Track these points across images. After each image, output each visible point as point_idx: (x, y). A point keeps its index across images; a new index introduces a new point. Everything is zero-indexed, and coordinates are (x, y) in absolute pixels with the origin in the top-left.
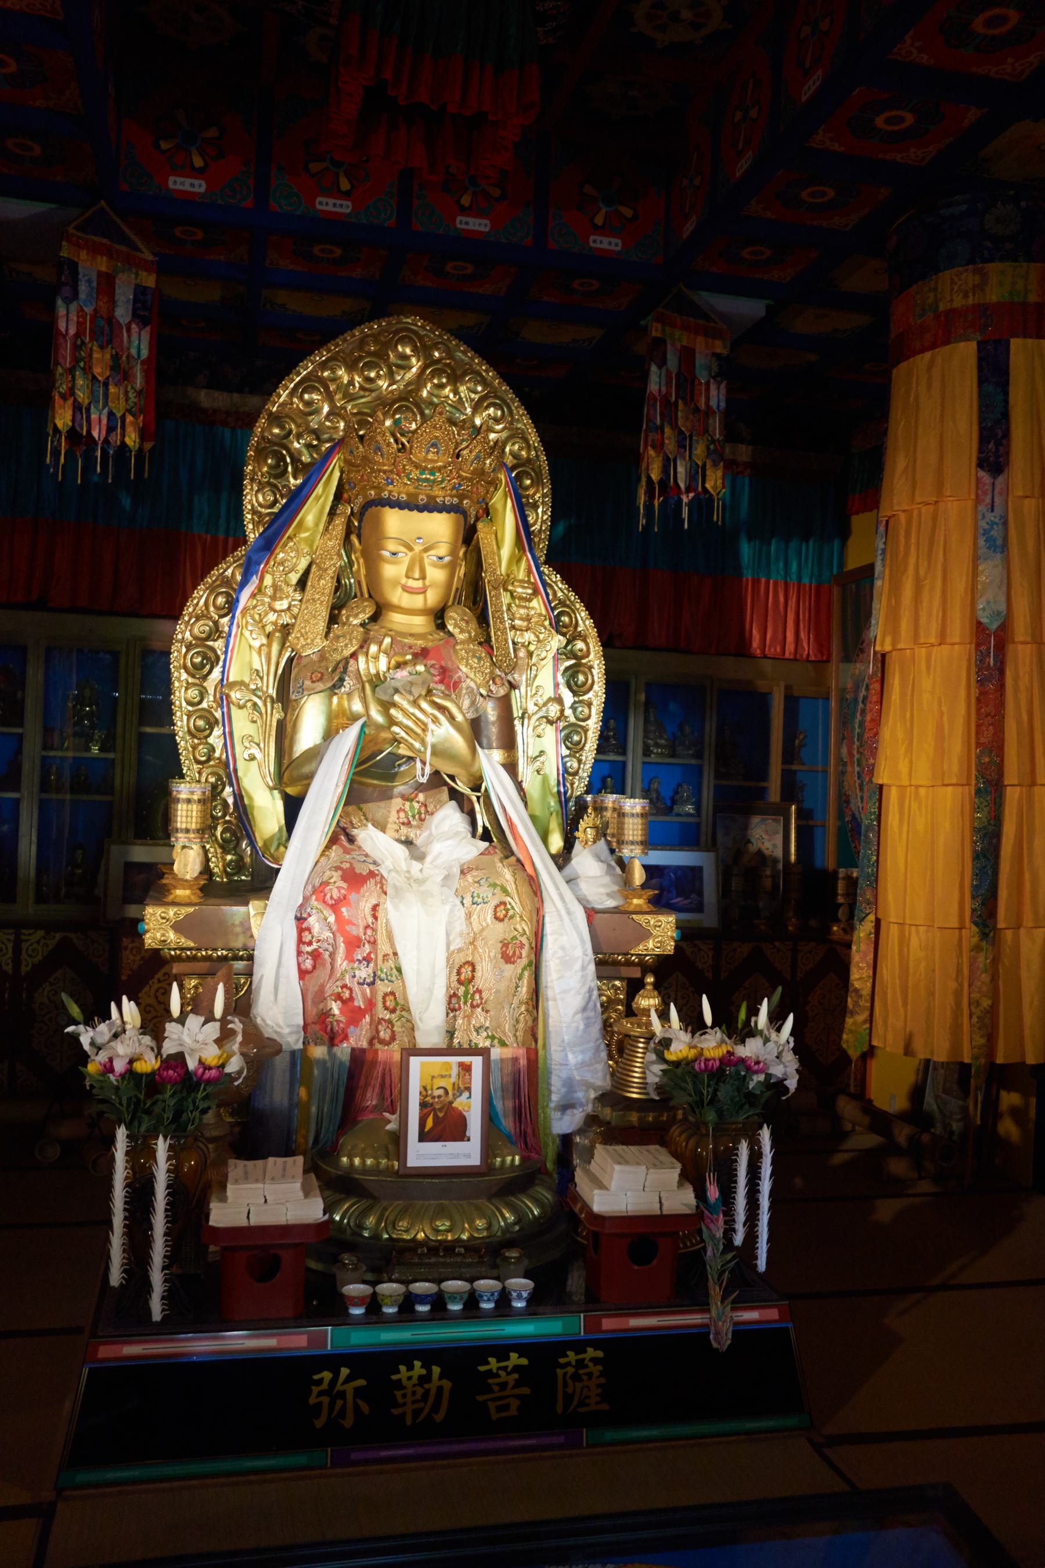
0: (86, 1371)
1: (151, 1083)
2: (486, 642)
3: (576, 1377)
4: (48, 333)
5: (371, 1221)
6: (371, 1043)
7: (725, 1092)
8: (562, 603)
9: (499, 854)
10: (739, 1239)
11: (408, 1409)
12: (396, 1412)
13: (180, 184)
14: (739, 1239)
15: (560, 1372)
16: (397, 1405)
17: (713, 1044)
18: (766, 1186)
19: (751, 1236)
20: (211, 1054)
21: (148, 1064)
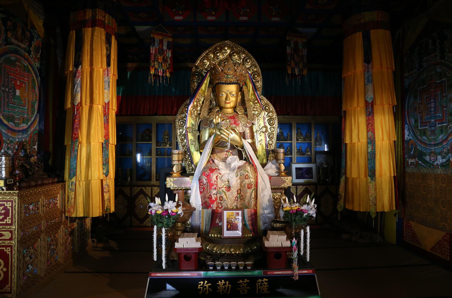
0: (149, 279)
1: (161, 216)
2: (247, 115)
3: (261, 285)
4: (149, 53)
5: (215, 249)
6: (216, 208)
7: (298, 218)
8: (266, 104)
9: (248, 164)
10: (302, 253)
11: (221, 291)
12: (218, 291)
13: (177, 18)
14: (302, 253)
15: (257, 284)
16: (218, 290)
17: (296, 206)
18: (308, 241)
19: (305, 253)
20: (174, 210)
21: (160, 212)
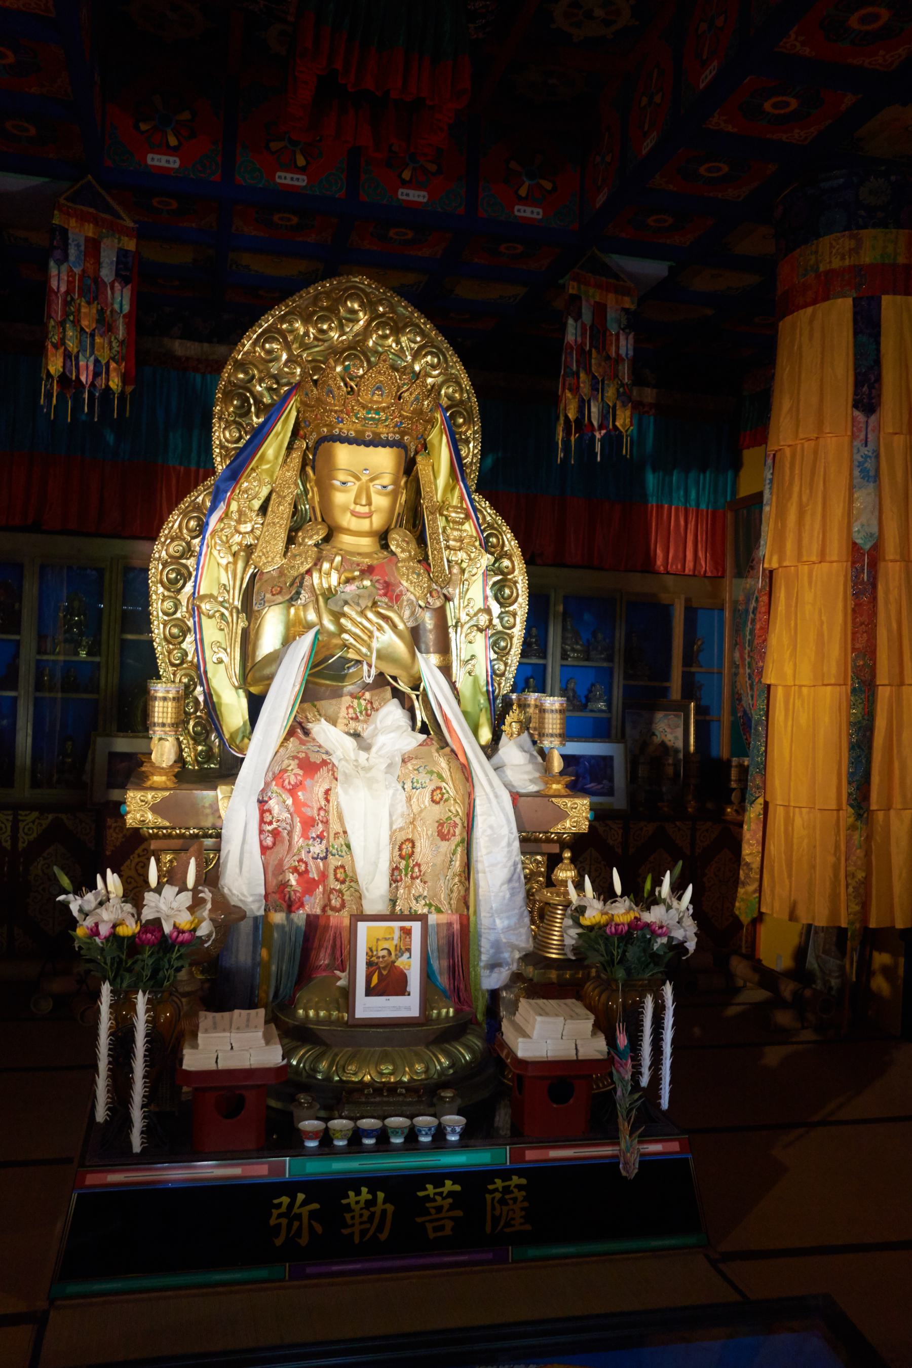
0: (75, 1196)
1: (132, 945)
2: (424, 561)
3: (503, 1202)
4: (42, 290)
5: (323, 1065)
6: (324, 910)
7: (633, 953)
8: (490, 526)
9: (436, 745)
10: (645, 1081)
11: (356, 1230)
12: (345, 1231)
13: (157, 160)
14: (645, 1081)
15: (488, 1197)
16: (347, 1226)
17: (623, 911)
18: (668, 1035)
19: (656, 1079)
20: (184, 920)
21: (130, 928)
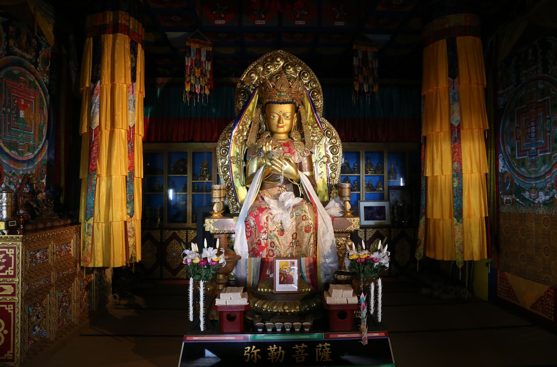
0: (183, 343)
1: (198, 266)
2: (304, 142)
3: (322, 351)
4: (183, 66)
5: (265, 306)
6: (267, 256)
7: (367, 268)
8: (328, 128)
9: (306, 202)
10: (372, 312)
11: (272, 358)
12: (269, 359)
13: (218, 22)
14: (372, 312)
15: (317, 350)
16: (269, 357)
17: (364, 254)
18: (380, 296)
19: (376, 311)
20: (215, 258)
21: (197, 261)
